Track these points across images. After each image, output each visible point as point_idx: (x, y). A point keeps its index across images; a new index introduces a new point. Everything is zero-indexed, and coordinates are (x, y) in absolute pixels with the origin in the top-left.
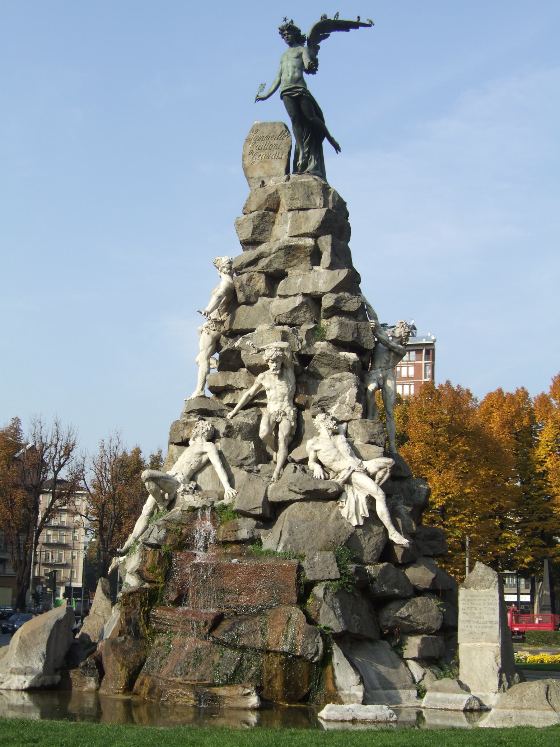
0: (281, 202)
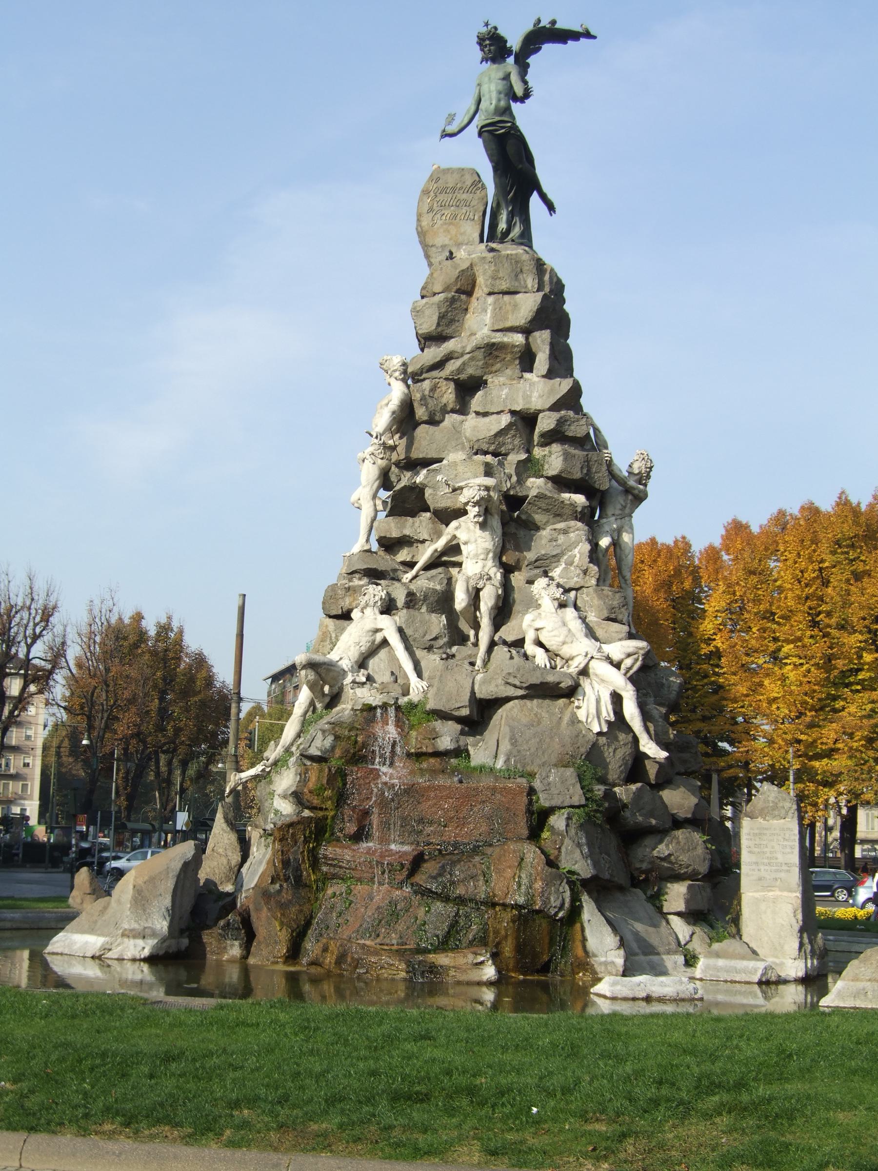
0: (478, 282)
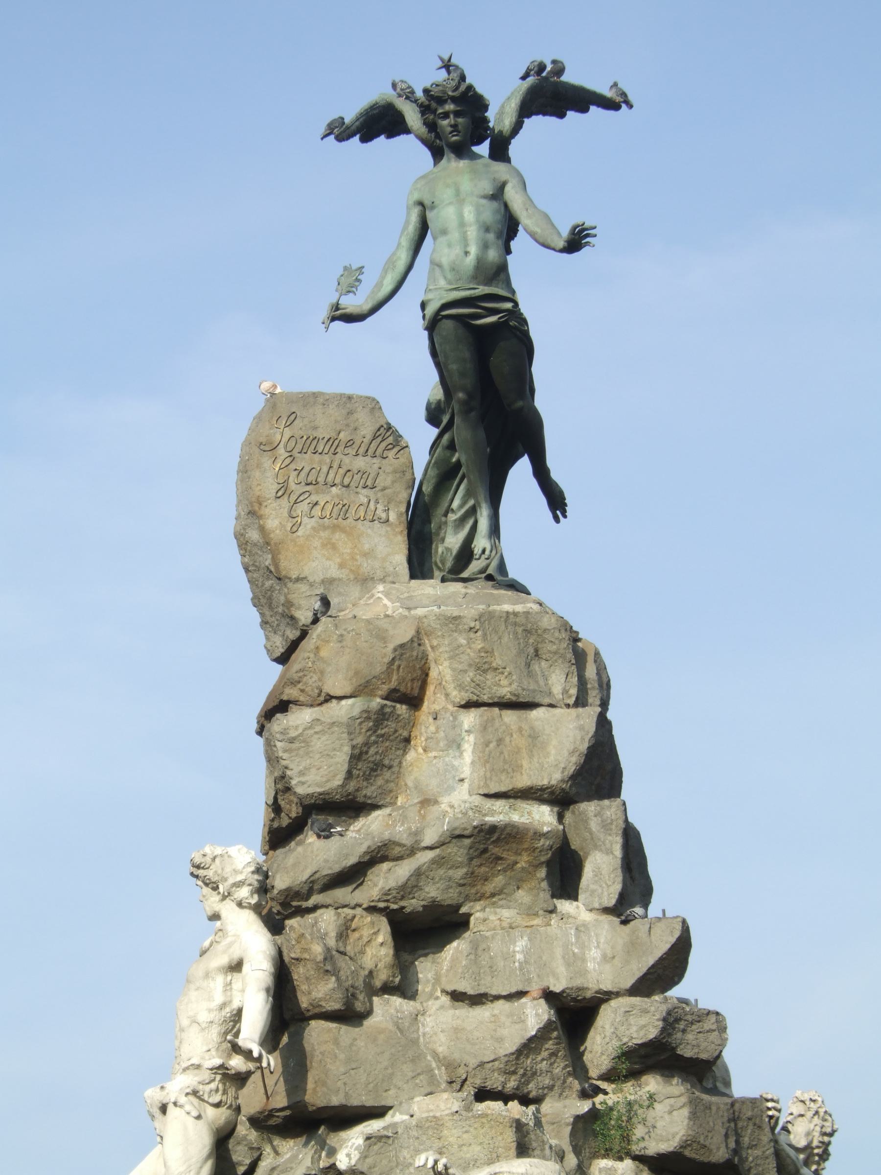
0: (433, 674)
